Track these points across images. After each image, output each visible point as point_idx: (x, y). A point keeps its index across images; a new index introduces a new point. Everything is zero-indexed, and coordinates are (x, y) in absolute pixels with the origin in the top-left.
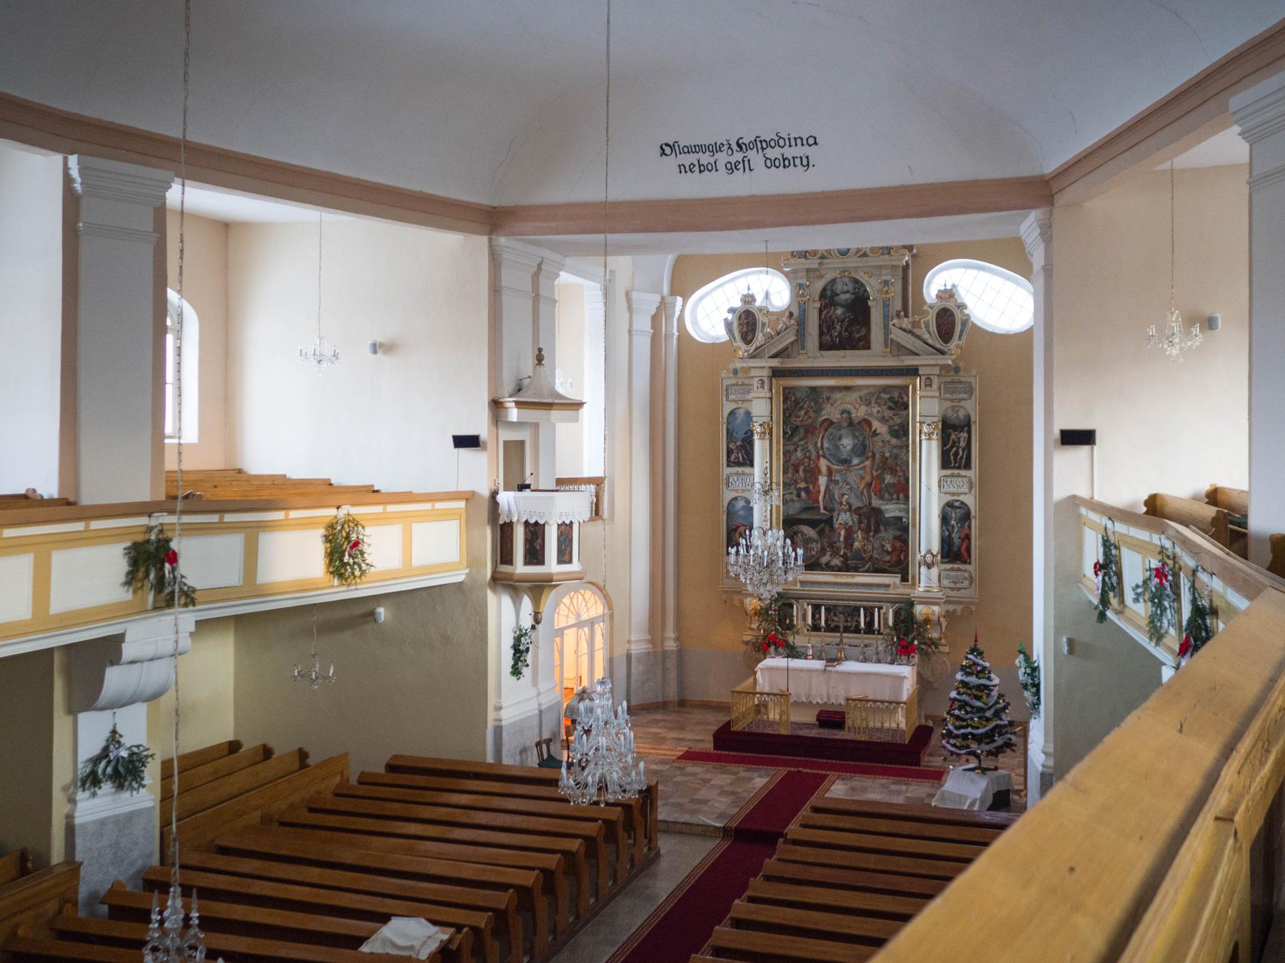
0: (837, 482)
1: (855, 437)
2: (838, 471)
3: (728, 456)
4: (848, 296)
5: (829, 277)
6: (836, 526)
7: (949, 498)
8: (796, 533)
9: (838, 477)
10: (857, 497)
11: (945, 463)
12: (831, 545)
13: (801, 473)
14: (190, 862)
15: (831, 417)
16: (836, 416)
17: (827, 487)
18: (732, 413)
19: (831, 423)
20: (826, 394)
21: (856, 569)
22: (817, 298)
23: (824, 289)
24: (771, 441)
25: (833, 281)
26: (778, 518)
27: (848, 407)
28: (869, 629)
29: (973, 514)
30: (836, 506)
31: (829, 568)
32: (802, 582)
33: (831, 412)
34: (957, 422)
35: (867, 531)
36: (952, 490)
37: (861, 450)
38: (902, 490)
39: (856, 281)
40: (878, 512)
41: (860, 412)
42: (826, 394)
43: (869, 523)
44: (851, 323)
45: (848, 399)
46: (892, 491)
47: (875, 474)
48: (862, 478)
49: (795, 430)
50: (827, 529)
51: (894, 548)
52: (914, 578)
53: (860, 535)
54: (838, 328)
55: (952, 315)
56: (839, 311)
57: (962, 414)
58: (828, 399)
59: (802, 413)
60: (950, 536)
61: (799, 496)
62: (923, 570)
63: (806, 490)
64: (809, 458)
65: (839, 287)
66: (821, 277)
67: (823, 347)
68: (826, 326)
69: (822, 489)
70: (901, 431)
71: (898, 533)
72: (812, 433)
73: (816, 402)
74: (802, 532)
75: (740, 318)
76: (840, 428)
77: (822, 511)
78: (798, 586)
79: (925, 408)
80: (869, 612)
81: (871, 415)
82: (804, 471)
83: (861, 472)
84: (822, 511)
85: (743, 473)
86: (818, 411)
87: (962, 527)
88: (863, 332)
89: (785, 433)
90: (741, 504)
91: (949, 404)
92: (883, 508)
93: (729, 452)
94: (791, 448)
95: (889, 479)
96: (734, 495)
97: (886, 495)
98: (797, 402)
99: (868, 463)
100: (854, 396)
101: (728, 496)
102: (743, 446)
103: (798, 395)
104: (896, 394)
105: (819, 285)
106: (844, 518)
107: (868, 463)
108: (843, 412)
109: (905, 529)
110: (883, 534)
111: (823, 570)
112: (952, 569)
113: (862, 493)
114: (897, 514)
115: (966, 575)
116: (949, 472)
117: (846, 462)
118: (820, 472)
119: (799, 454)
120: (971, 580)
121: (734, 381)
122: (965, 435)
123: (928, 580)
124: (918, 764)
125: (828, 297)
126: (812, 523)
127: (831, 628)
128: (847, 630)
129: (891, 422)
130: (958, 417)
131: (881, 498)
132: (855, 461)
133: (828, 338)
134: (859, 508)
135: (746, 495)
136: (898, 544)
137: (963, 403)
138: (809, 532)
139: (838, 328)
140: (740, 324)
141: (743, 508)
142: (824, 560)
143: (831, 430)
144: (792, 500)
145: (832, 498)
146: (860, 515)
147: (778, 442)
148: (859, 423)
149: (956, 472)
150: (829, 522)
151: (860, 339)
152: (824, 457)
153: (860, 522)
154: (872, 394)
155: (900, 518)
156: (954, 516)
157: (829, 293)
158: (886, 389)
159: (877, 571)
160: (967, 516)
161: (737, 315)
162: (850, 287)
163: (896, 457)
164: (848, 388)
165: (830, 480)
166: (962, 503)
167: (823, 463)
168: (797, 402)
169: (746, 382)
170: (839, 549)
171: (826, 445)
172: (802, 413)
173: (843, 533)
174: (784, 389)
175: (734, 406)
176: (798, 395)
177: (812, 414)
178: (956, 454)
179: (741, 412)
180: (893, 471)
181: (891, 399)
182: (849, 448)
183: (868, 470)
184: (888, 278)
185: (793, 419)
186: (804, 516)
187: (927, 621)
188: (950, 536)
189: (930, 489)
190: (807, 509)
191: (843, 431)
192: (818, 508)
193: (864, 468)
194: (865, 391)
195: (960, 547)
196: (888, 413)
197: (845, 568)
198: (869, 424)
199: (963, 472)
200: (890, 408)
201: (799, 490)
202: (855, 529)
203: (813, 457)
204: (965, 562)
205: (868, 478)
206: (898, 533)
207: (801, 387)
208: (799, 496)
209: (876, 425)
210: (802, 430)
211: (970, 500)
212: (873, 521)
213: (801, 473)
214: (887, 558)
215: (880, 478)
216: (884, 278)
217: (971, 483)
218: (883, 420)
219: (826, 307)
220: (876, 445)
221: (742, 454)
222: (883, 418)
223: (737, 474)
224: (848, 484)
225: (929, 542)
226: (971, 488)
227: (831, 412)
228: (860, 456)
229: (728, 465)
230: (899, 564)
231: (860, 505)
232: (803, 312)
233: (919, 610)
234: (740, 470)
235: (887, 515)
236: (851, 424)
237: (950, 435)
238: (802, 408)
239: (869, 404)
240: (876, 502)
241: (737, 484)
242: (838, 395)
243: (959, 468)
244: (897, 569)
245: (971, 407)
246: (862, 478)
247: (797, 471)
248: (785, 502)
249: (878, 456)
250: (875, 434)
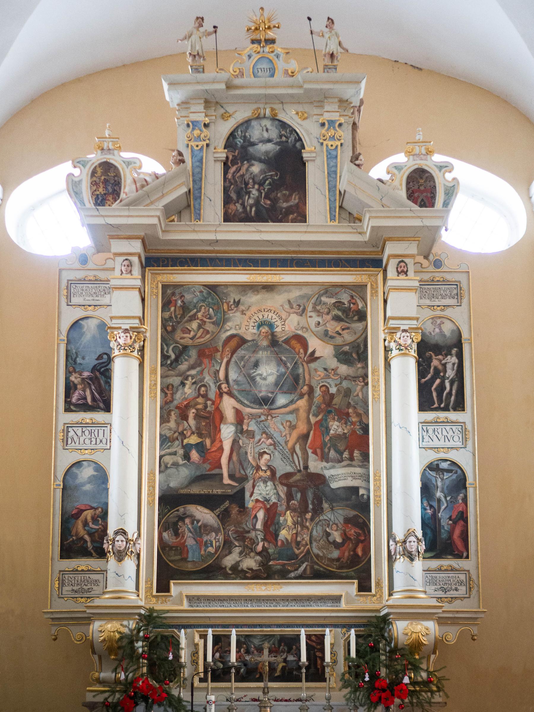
0: (251, 435)
1: (280, 362)
2: (252, 416)
4: (269, 146)
5: (242, 114)
6: (250, 504)
8: (182, 518)
9: (252, 426)
10: (284, 457)
11: (425, 403)
12: (242, 536)
13: (192, 421)
14: (444, 670)
16: (249, 332)
17: (235, 442)
18: (76, 325)
19: (243, 341)
20: (234, 296)
21: (283, 574)
22: (222, 143)
23: (232, 135)
24: (141, 365)
26: (151, 494)
28: (316, 672)
29: (470, 480)
30: (250, 472)
31: (238, 573)
32: (191, 598)
33: (241, 324)
34: (440, 341)
36: (436, 443)
37: (292, 383)
38: (356, 445)
39: (283, 125)
40: (319, 480)
41: (288, 325)
42: (234, 296)
43: (304, 500)
44: (276, 186)
45: (269, 304)
46: (341, 446)
47: (313, 420)
48: (293, 427)
49: (182, 351)
50: (235, 510)
51: (346, 537)
52: (379, 584)
53: (288, 518)
54: (255, 192)
55: (431, 178)
56: (256, 168)
57: (447, 328)
58: (237, 303)
59: (194, 325)
60: (434, 515)
61: (187, 457)
63: (200, 447)
64: (205, 396)
65: (256, 133)
66: (225, 117)
67: (227, 218)
68: (234, 191)
69: (227, 446)
70: (355, 354)
72: (211, 357)
73: (218, 309)
74: (191, 516)
76: (256, 347)
77: (226, 481)
78: (185, 606)
79: (399, 307)
80: (316, 644)
81: (306, 329)
82: (197, 417)
83: (290, 417)
84: (226, 481)
85: (94, 424)
86: (220, 323)
87: (454, 501)
88: (294, 200)
89: (165, 357)
90: (87, 472)
91: (429, 313)
92: (327, 473)
93: (69, 388)
94: (176, 381)
95: (336, 427)
96: (76, 457)
97: (332, 454)
98: (185, 308)
99: (302, 403)
100: (278, 300)
101: (65, 459)
102: (93, 379)
103: (188, 297)
104: (345, 298)
105: (224, 129)
106: (262, 491)
107: (302, 403)
108: (260, 325)
109: (364, 506)
110: (328, 515)
111: (227, 576)
112: (440, 569)
115: (462, 577)
116: (430, 416)
117: (266, 402)
118: (222, 418)
119: (189, 390)
120: (469, 584)
121: (80, 275)
122: (454, 360)
123: (407, 582)
125: (238, 148)
126: (208, 501)
127: (249, 673)
129: (339, 340)
130: (442, 333)
131: (324, 458)
132: (282, 400)
133: (239, 207)
134: (288, 475)
135: (97, 457)
136: (352, 531)
137: (448, 312)
138: (204, 515)
139: (255, 192)
140: (94, 184)
141: (91, 480)
142: (229, 561)
143: (241, 352)
145: (242, 462)
147: (153, 371)
149: (442, 415)
150: (238, 498)
151: (289, 210)
152: (230, 394)
153: (290, 496)
155: (355, 490)
156: (445, 485)
157: (239, 141)
158: (329, 289)
159: (318, 575)
160: (460, 484)
161: (88, 170)
162: (274, 134)
163: (348, 393)
164: (269, 288)
165: (240, 430)
166: (453, 463)
167: (228, 405)
168: (185, 308)
169: (102, 275)
170: (254, 542)
171: (233, 375)
172: (194, 325)
173: (261, 515)
174: (165, 287)
175: (79, 313)
176: (188, 297)
177: (209, 327)
178: (441, 388)
179: (90, 326)
180: (343, 416)
181: (338, 305)
182: (271, 379)
183: (302, 414)
184: (335, 116)
185: (178, 334)
186: (195, 490)
187: (416, 646)
188: (434, 515)
189: (405, 445)
191: (261, 355)
193: (296, 410)
194: (295, 293)
195: (451, 533)
196: (333, 327)
197: (265, 573)
198: (303, 342)
199: (452, 415)
200: (337, 318)
201: (187, 449)
202: (282, 508)
203: (212, 395)
204: (459, 556)
205: (302, 428)
206: (352, 513)
207: (194, 284)
208: (187, 457)
209: (314, 344)
210: (193, 353)
211: (464, 459)
212: (310, 495)
214: (336, 554)
215: (322, 427)
216: (327, 116)
217: (464, 431)
218: (326, 336)
219: (234, 162)
220: (315, 375)
221: (91, 389)
222: (326, 333)
223: (81, 424)
225: (407, 516)
226: (465, 440)
227: (241, 324)
228: (289, 392)
229: (68, 410)
230: (355, 566)
231: (289, 469)
233: (401, 629)
235: (334, 485)
236: (274, 342)
237: (430, 359)
238: (194, 318)
239: (303, 312)
240: (315, 465)
241: (81, 438)
244: (351, 572)
245: (459, 317)
246: (293, 427)
247: (185, 417)
248: (164, 468)
249: (318, 392)
250: (313, 358)
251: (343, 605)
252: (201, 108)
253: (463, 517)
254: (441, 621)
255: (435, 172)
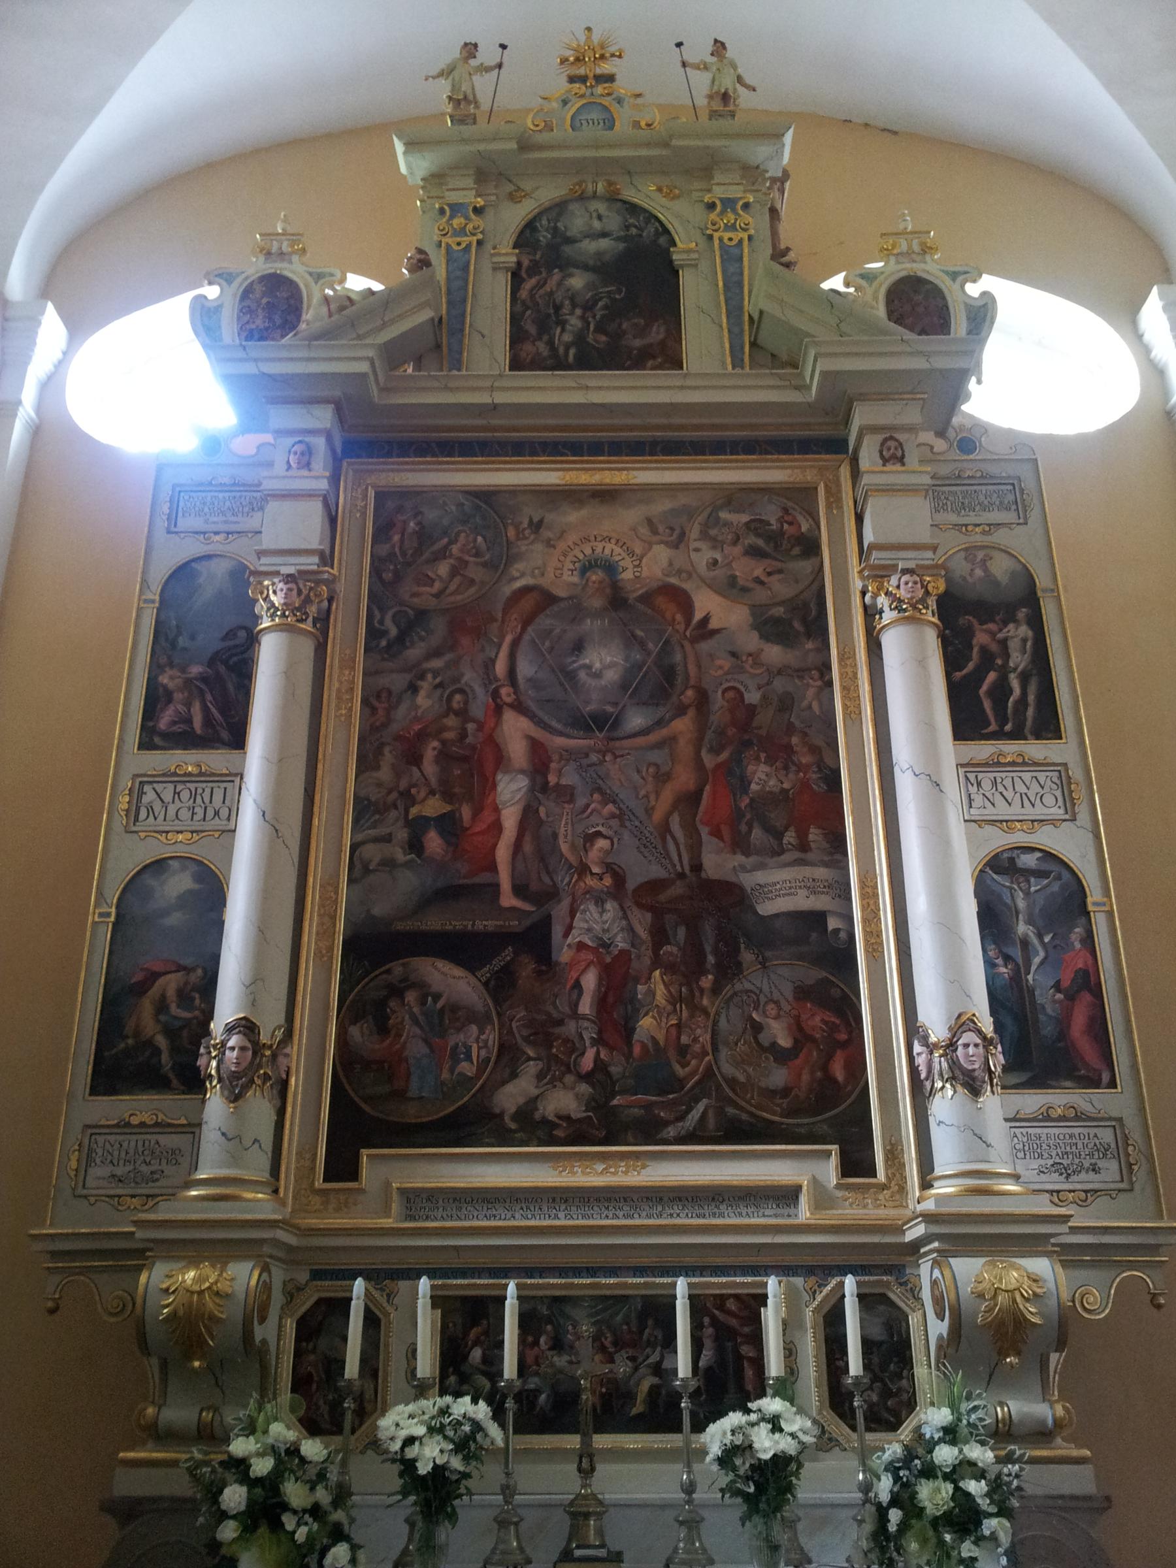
0: (566, 794)
1: (631, 641)
2: (570, 755)
3: (150, 712)
4: (604, 243)
6: (563, 955)
7: (998, 840)
9: (570, 777)
11: (968, 722)
12: (544, 1033)
13: (430, 767)
15: (546, 582)
17: (529, 814)
19: (547, 599)
20: (530, 511)
21: (648, 1130)
23: (530, 226)
25: (559, 208)
26: (326, 933)
27: (609, 550)
29: (1094, 895)
30: (563, 879)
31: (533, 1129)
35: (688, 970)
37: (658, 683)
38: (813, 816)
40: (729, 899)
41: (653, 565)
42: (530, 511)
49: (414, 622)
50: (527, 968)
51: (802, 1037)
53: (658, 987)
54: (574, 322)
56: (577, 281)
57: (1000, 568)
58: (537, 526)
59: (443, 569)
60: (1017, 979)
61: (415, 846)
62: (946, 1104)
63: (448, 825)
64: (463, 714)
65: (577, 221)
69: (510, 819)
71: (813, 975)
75: (247, 293)
77: (508, 899)
78: (480, 734)
81: (690, 573)
82: (445, 757)
84: (508, 899)
86: (501, 560)
87: (1057, 949)
89: (374, 633)
90: (179, 883)
92: (748, 880)
94: (397, 681)
95: (763, 777)
97: (757, 834)
99: (683, 725)
103: (431, 515)
104: (771, 514)
105: (514, 216)
107: (683, 725)
108: (587, 567)
109: (841, 959)
110: (753, 980)
111: (505, 1139)
112: (1046, 1117)
113: (665, 829)
114: (803, 902)
116: (983, 750)
117: (602, 723)
118: (500, 760)
119: (424, 700)
122: (1024, 631)
123: (965, 1144)
124: (311, 1271)
126: (463, 949)
128: (614, 1412)
129: (761, 596)
131: (740, 844)
132: (636, 720)
134: (654, 886)
135: (203, 851)
136: (817, 1020)
139: (574, 322)
141: (184, 901)
142: (510, 1097)
143: (544, 621)
144: (389, 864)
145: (546, 853)
146: (658, 912)
148: (646, 598)
149: (1010, 748)
150: (536, 940)
152: (519, 707)
153: (660, 936)
154: (689, 513)
155: (817, 918)
156: (1023, 902)
157: (544, 237)
158: (733, 496)
160: (1070, 904)
161: (237, 287)
162: (613, 222)
164: (605, 495)
166: (1048, 856)
167: (515, 732)
170: (574, 1048)
171: (526, 669)
172: (443, 569)
173: (590, 981)
177: (475, 572)
178: (1001, 691)
180: (779, 752)
181: (756, 526)
182: (611, 676)
183: (684, 747)
186: (434, 922)
188: (1017, 979)
190: (450, 894)
192: (496, 887)
195: (1063, 1022)
196: (747, 569)
197: (601, 1127)
199: (1035, 749)
200: (754, 552)
201: (417, 828)
203: (480, 705)
204: (1092, 1082)
205: (684, 779)
206: (813, 975)
208: (415, 846)
209: (706, 603)
210: (439, 626)
211: (1070, 844)
213: (430, 767)
214: (778, 1077)
217: (1065, 783)
218: (732, 588)
219: (534, 269)
222: (732, 581)
223: (174, 777)
224: (609, 798)
227: (548, 566)
229: (146, 744)
231: (656, 871)
232: (460, 269)
234: (187, 760)
235: (766, 908)
236: (617, 600)
237: (969, 633)
238: (442, 555)
239: (679, 541)
240: (718, 862)
242: (573, 516)
243: (1017, 734)
246: (663, 778)
247: (414, 758)
249: (718, 701)
250: (704, 631)
251: (804, 1212)
252: (469, 182)
253: (1087, 983)
254: (1069, 1256)
255: (944, 283)
